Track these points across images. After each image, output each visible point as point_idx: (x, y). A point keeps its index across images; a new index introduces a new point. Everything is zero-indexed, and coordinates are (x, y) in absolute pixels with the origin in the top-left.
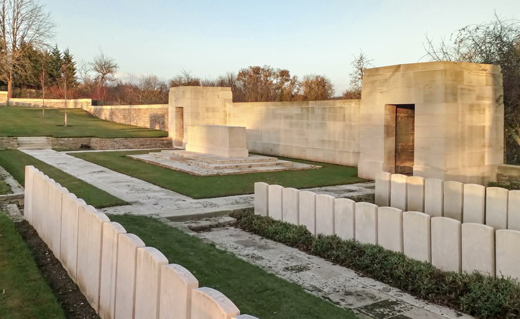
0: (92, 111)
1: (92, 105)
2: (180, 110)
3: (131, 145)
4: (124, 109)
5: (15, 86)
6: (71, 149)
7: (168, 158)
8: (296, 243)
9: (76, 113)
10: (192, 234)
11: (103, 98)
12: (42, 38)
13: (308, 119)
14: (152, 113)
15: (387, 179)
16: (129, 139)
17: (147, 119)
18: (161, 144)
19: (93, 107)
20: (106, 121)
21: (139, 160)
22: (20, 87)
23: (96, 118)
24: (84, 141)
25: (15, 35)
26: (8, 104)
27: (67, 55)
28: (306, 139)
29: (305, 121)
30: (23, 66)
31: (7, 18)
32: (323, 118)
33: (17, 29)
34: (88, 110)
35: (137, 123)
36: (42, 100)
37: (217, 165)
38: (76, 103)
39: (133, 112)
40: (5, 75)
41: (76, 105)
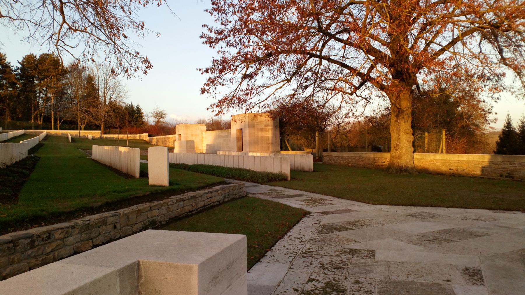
4: (162, 138)
5: (106, 128)
22: (109, 128)
30: (110, 116)
33: (107, 94)
38: (140, 136)
39: (166, 139)
40: (100, 121)
41: (140, 138)
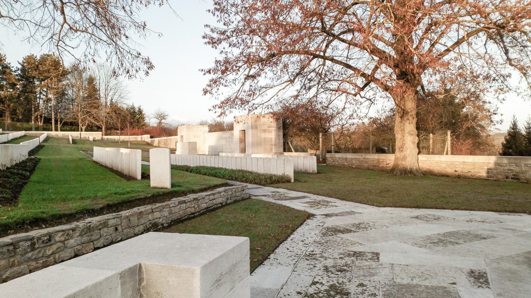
0: (150, 142)
4: (164, 140)
5: (107, 129)
12: (122, 100)
19: (150, 139)
25: (106, 98)
30: (111, 117)
34: (148, 141)
36: (128, 137)
38: (142, 138)
39: (168, 141)
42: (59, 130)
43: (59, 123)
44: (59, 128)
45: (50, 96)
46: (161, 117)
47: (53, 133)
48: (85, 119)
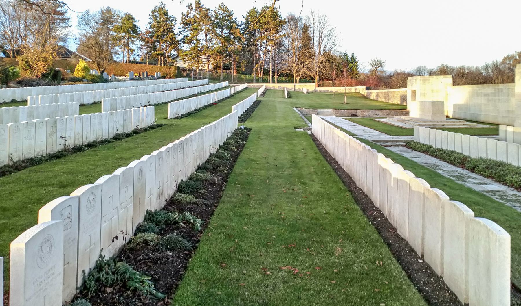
0: (366, 94)
1: (366, 90)
2: (414, 92)
3: (381, 114)
4: (385, 92)
5: (320, 79)
6: (345, 116)
7: (396, 120)
8: (425, 151)
9: (356, 96)
10: (374, 143)
11: (374, 85)
12: (336, 47)
13: (499, 96)
14: (401, 94)
15: (505, 129)
16: (379, 111)
17: (399, 98)
18: (401, 114)
19: (367, 91)
20: (374, 100)
21: (379, 122)
22: (323, 80)
23: (368, 98)
24: (353, 112)
25: (320, 47)
26: (315, 91)
27: (353, 56)
28: (498, 110)
29: (497, 98)
30: (324, 67)
31: (315, 37)
32: (508, 96)
35: (392, 101)
37: (420, 124)
38: (356, 89)
39: (390, 94)
41: (356, 91)
42: (276, 81)
43: (276, 74)
44: (276, 79)
45: (269, 48)
46: (378, 64)
47: (271, 85)
48: (299, 69)
